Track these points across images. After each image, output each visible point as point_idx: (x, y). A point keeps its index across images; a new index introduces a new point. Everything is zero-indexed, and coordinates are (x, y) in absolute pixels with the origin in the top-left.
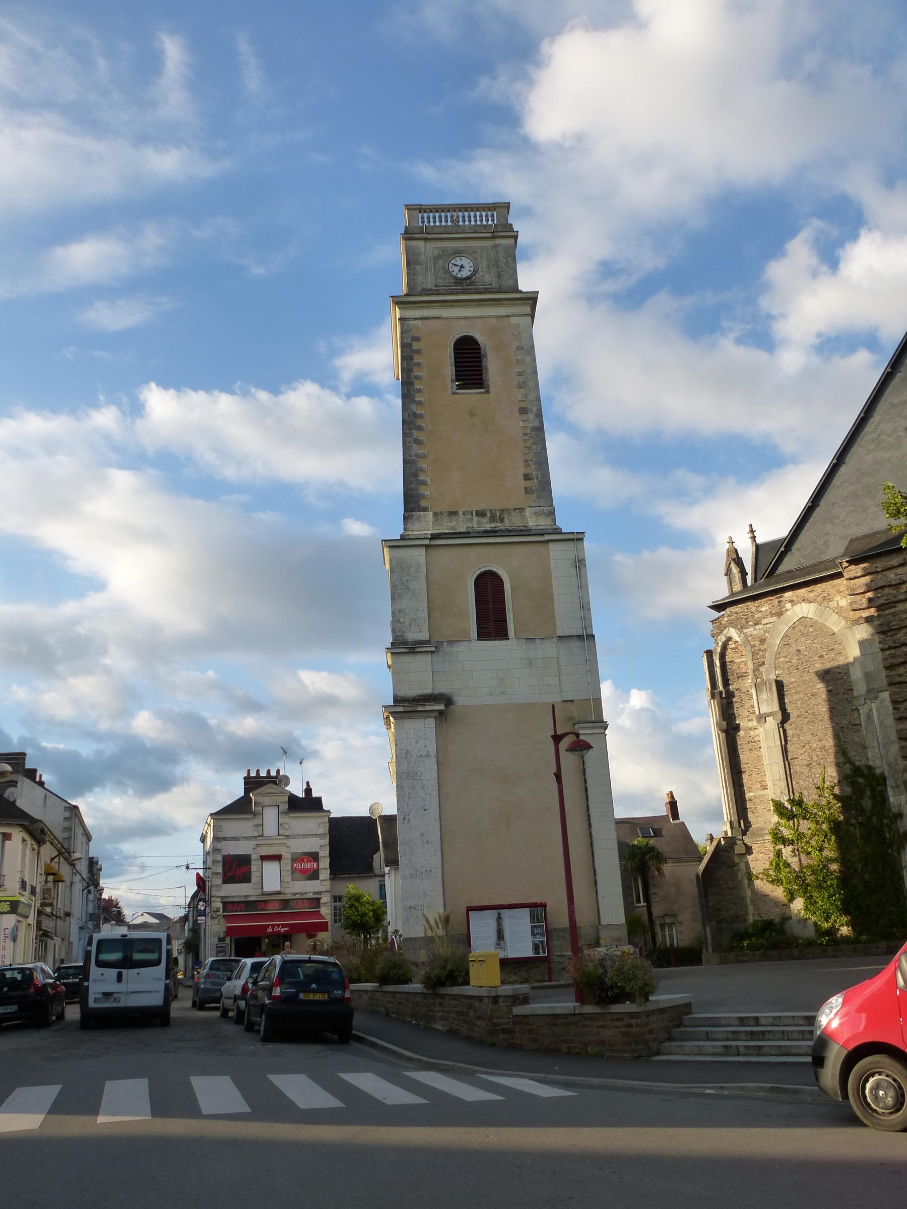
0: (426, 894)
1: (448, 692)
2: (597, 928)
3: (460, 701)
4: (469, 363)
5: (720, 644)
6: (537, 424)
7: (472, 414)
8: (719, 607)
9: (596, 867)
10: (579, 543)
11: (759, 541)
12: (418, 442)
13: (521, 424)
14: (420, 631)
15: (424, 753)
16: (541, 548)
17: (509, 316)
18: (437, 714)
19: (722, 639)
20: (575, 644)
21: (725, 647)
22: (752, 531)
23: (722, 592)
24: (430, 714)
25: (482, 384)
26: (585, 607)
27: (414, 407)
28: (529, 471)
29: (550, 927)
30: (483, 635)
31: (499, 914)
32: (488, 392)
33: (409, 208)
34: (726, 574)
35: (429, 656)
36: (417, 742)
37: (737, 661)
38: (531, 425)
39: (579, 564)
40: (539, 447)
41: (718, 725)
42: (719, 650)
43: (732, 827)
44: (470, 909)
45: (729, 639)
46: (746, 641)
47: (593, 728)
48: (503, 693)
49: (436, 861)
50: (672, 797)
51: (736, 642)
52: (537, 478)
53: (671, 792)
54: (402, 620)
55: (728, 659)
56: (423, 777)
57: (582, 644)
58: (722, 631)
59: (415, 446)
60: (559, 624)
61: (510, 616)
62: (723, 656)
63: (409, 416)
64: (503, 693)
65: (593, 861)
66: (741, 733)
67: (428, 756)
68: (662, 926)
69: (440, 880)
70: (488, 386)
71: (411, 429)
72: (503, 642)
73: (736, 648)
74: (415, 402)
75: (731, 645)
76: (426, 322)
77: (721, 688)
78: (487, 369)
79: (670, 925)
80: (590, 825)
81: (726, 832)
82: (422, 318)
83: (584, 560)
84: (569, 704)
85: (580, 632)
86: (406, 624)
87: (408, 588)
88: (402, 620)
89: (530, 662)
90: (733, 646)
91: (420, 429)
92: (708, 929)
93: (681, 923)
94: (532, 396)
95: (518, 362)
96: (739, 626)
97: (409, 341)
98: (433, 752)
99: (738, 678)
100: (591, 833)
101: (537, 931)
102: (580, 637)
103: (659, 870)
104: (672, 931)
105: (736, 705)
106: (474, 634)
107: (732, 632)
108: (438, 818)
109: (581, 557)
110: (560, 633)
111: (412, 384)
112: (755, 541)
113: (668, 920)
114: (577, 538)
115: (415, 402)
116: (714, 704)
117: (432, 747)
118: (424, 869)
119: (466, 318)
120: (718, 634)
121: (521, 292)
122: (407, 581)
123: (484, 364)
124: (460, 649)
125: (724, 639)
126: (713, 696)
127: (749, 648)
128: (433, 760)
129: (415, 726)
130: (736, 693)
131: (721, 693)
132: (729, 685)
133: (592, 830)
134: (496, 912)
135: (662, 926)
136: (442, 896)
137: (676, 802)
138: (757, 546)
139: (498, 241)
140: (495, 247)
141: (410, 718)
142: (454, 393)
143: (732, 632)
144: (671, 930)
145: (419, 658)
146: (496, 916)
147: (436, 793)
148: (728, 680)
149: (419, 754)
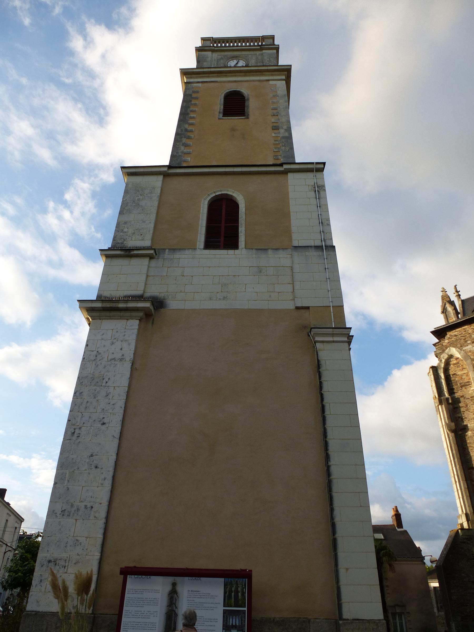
0: (76, 543)
1: (161, 296)
2: (337, 623)
3: (173, 305)
4: (235, 105)
5: (443, 361)
6: (287, 134)
8: (440, 333)
9: (337, 519)
10: (318, 174)
11: (463, 298)
12: (186, 145)
13: (273, 135)
14: (143, 240)
15: (118, 356)
16: (280, 178)
17: (268, 80)
18: (141, 314)
19: (444, 356)
20: (313, 253)
21: (447, 363)
22: (457, 292)
23: (441, 322)
24: (134, 314)
25: (244, 114)
26: (324, 223)
27: (186, 126)
29: (255, 615)
30: (209, 245)
31: (174, 585)
32: (248, 118)
34: (443, 312)
35: (146, 261)
36: (113, 343)
37: (459, 373)
38: (281, 135)
39: (319, 190)
40: (287, 149)
41: (448, 426)
42: (443, 365)
43: (468, 520)
44: (127, 572)
45: (451, 356)
46: (466, 356)
47: (333, 335)
48: (224, 298)
49: (103, 495)
50: (397, 511)
51: (457, 359)
53: (396, 507)
54: (126, 230)
55: (451, 372)
56: (110, 383)
57: (320, 253)
58: (443, 351)
59: (182, 148)
60: (294, 236)
61: (242, 230)
62: (446, 370)
63: (182, 130)
64: (224, 298)
65: (332, 510)
66: (469, 433)
67: (121, 360)
68: (394, 614)
69: (101, 523)
70: (248, 115)
71: (182, 138)
72: (231, 252)
73: (458, 363)
74: (188, 123)
75: (453, 361)
76: (205, 84)
77: (447, 395)
78: (248, 106)
79: (400, 615)
80: (327, 457)
81: (462, 525)
82: (202, 82)
83: (324, 186)
84: (303, 311)
85: (318, 243)
87: (138, 205)
89: (260, 270)
90: (455, 362)
91: (189, 138)
92: (453, 625)
93: (408, 613)
94: (284, 120)
95: (273, 103)
96: (459, 345)
97: (191, 93)
99: (462, 387)
100: (328, 467)
101: (234, 621)
102: (319, 248)
103: (390, 565)
104: (402, 620)
105: (462, 409)
106: (201, 244)
107: (454, 351)
108: (117, 436)
109: (320, 183)
110: (295, 243)
111: (188, 114)
112: (460, 298)
113: (398, 610)
114: (318, 168)
115: (188, 123)
116: (442, 409)
117: (129, 351)
118: (82, 505)
119: (235, 81)
120: (441, 353)
121: (275, 45)
122: (139, 200)
123: (246, 104)
124: (184, 258)
125: (446, 357)
126: (441, 403)
127: (469, 361)
128: (127, 366)
129: (111, 326)
130: (462, 399)
131: (447, 399)
132: (454, 393)
133: (331, 463)
134: (170, 580)
135: (394, 614)
136: (99, 549)
137: (400, 515)
138: (463, 301)
139: (264, 51)
140: (262, 54)
141: (110, 318)
142: (219, 119)
143: (454, 351)
144: (401, 619)
145: (135, 261)
146: (169, 588)
147: (121, 403)
148: (453, 389)
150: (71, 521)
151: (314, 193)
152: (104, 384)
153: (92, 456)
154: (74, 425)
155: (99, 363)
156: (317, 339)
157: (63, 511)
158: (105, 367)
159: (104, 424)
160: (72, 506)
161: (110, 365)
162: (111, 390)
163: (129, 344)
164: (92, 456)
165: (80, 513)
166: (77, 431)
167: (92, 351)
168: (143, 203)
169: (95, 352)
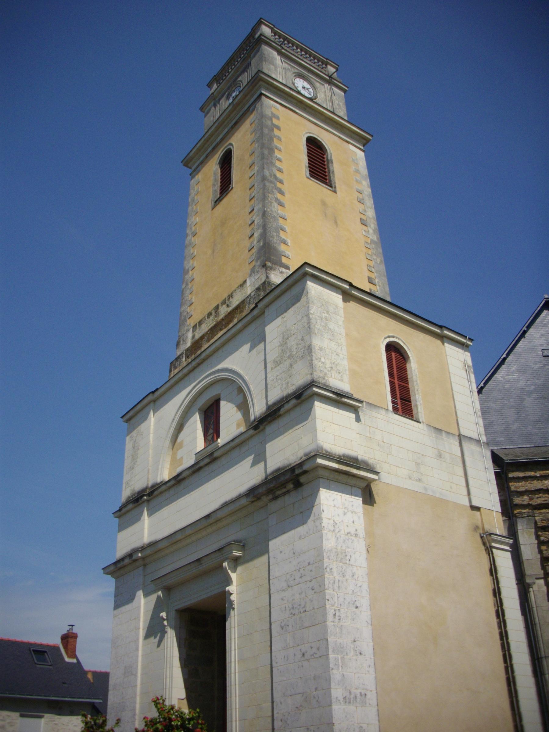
7: (324, 204)
28: (373, 276)
33: (103, 569)
52: (379, 286)
54: (323, 360)
86: (328, 365)
88: (323, 360)
95: (357, 181)
97: (270, 115)
98: (362, 533)
149: (347, 530)
150: (351, 708)
151: (465, 372)
152: (348, 562)
153: (355, 641)
154: (333, 605)
155: (338, 536)
156: (494, 545)
157: (345, 698)
158: (344, 541)
159: (357, 607)
160: (350, 693)
161: (348, 540)
162: (355, 570)
163: (359, 518)
164: (355, 641)
165: (358, 700)
166: (337, 614)
167: (329, 519)
168: (331, 325)
169: (332, 522)
